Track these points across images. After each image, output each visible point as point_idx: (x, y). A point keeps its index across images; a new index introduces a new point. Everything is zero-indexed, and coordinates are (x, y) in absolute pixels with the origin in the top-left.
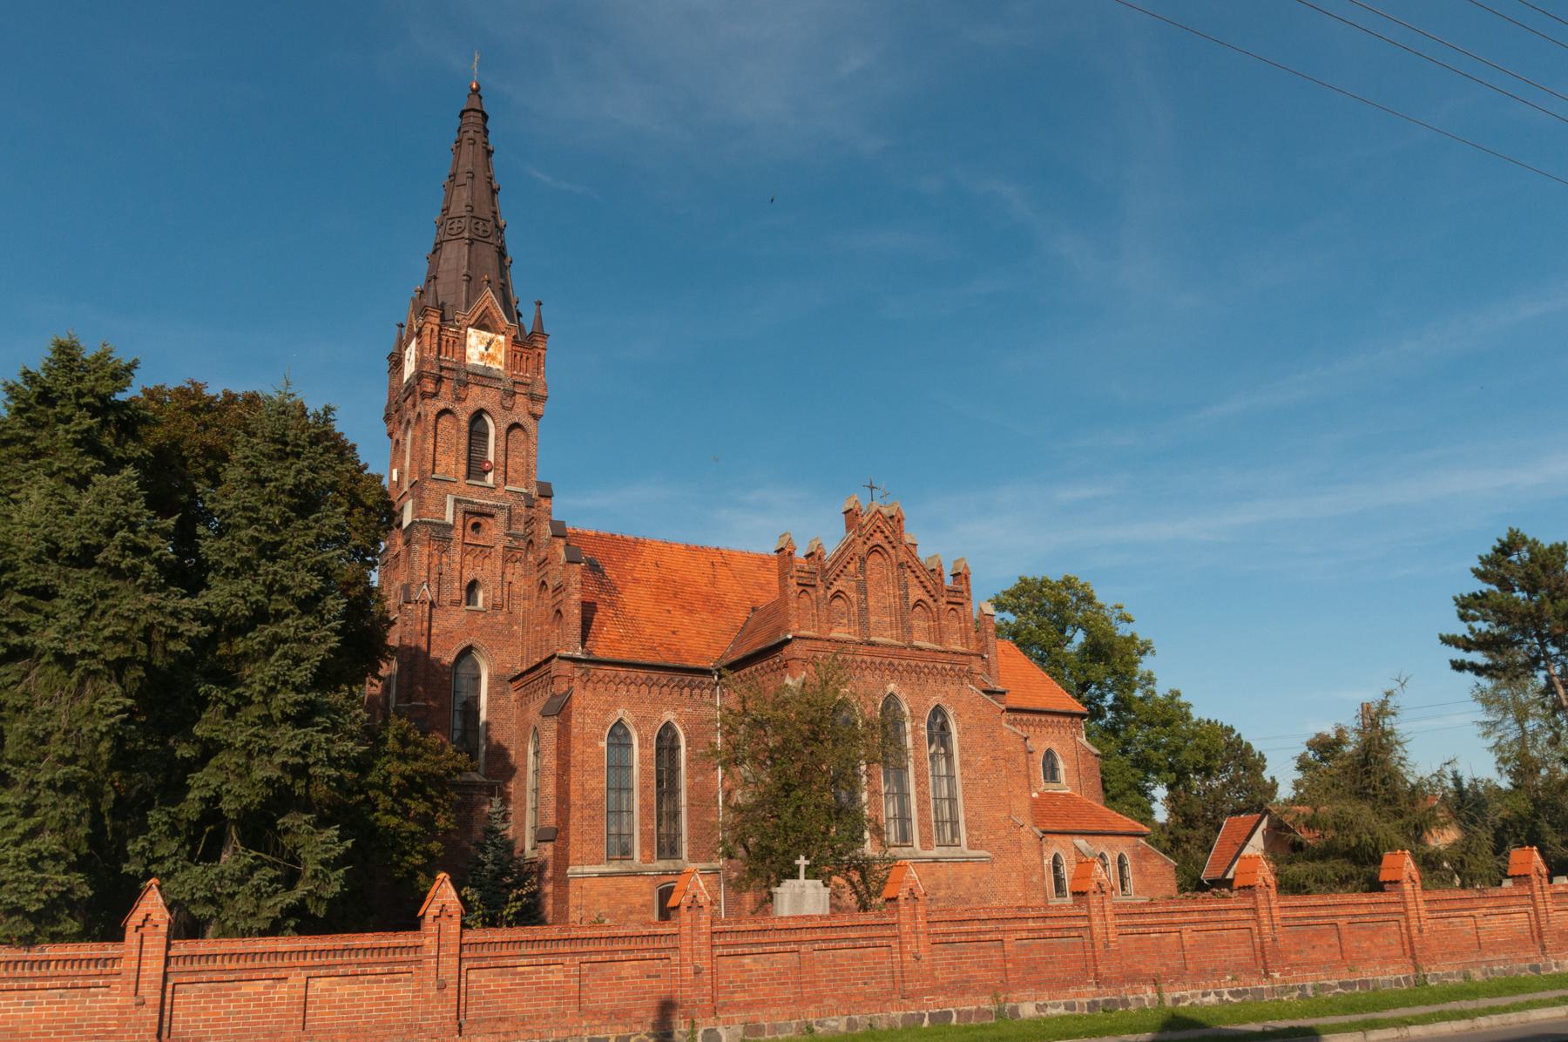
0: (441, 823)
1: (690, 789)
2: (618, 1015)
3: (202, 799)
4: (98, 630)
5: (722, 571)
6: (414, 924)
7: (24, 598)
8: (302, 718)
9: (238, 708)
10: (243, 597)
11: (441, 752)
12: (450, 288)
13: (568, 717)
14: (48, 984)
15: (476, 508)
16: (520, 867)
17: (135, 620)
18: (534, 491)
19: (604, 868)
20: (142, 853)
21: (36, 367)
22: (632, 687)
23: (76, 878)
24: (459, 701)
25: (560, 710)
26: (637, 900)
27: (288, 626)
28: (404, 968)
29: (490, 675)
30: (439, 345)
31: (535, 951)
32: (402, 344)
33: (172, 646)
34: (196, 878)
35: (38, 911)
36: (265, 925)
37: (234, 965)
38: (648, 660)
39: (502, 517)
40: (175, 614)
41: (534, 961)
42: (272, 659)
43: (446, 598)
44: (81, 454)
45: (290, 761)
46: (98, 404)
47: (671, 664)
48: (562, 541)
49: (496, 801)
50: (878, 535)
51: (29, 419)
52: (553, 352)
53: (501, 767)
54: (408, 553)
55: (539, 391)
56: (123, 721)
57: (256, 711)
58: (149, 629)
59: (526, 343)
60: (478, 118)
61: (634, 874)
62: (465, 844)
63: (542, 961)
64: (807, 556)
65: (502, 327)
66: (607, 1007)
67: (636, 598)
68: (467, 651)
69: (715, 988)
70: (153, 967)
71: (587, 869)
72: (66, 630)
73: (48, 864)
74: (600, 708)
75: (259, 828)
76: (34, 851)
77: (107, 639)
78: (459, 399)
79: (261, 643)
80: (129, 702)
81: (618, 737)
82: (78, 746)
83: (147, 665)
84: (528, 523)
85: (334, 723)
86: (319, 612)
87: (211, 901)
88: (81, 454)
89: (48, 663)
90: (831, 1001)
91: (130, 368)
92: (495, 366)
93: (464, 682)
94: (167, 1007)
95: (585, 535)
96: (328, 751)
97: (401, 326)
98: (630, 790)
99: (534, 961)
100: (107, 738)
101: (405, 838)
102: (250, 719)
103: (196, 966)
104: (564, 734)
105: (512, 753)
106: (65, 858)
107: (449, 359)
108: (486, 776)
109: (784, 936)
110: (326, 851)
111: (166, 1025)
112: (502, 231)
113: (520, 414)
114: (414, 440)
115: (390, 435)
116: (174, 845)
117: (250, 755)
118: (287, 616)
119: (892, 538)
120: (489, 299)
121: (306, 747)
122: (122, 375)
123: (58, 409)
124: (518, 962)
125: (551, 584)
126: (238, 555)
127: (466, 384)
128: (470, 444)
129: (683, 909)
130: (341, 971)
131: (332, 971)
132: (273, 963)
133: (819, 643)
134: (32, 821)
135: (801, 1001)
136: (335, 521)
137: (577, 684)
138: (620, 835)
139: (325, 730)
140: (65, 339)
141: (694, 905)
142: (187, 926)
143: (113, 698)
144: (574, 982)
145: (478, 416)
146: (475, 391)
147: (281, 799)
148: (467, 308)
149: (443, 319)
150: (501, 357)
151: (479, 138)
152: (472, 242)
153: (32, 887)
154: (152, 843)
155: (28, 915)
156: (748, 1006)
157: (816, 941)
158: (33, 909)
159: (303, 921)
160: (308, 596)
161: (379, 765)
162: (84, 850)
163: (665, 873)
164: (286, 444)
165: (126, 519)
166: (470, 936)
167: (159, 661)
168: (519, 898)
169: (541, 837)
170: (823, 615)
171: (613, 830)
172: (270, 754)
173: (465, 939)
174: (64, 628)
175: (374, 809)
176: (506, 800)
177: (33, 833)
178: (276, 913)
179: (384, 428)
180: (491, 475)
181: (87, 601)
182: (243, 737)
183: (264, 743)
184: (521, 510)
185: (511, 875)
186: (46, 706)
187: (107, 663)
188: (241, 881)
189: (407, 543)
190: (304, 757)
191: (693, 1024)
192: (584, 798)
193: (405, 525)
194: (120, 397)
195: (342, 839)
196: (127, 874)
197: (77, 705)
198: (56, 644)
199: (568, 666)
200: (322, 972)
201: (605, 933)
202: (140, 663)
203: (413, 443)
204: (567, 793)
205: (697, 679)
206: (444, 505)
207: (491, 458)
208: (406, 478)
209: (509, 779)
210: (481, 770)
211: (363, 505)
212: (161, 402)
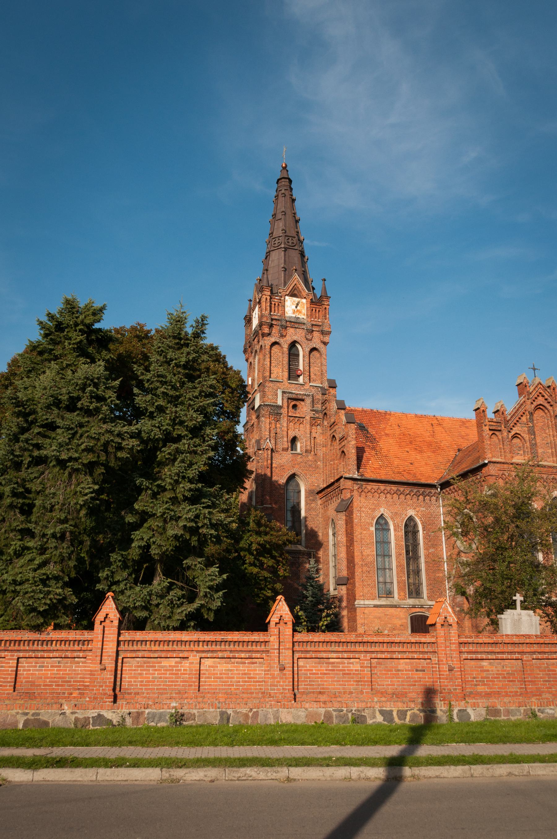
0: (281, 573)
1: (427, 556)
2: (398, 695)
3: (139, 547)
4: (79, 445)
5: (438, 429)
6: (264, 627)
7: (41, 429)
8: (194, 500)
9: (158, 493)
10: (159, 427)
11: (282, 530)
12: (275, 275)
13: (351, 513)
14: (51, 655)
15: (294, 396)
16: (328, 600)
17: (98, 440)
18: (326, 385)
19: (377, 602)
20: (107, 578)
21: (55, 311)
22: (388, 495)
23: (68, 591)
24: (290, 505)
25: (347, 508)
26: (398, 622)
27: (184, 444)
28: (258, 655)
29: (306, 490)
30: (271, 307)
31: (340, 649)
32: (251, 310)
33: (119, 454)
34: (136, 594)
35: (45, 611)
36: (177, 624)
37: (157, 648)
38: (397, 479)
39: (308, 401)
40: (119, 435)
41: (340, 655)
42: (176, 463)
43: (280, 447)
44: (78, 356)
45: (188, 525)
46: (86, 329)
47: (411, 481)
48: (343, 411)
49: (312, 561)
50: (540, 398)
51: (51, 339)
52: (332, 305)
53: (314, 543)
54: (259, 422)
55: (326, 329)
56: (92, 498)
57: (168, 495)
58: (106, 445)
59: (318, 302)
60: (285, 182)
61: (395, 606)
62: (296, 586)
63: (346, 655)
64: (495, 413)
65: (304, 294)
66: (390, 689)
67: (387, 444)
68: (292, 477)
69: (464, 681)
70: (111, 647)
71: (367, 602)
72: (60, 445)
73: (52, 583)
74: (369, 508)
75: (173, 565)
76: (44, 574)
77: (83, 450)
78: (282, 336)
79: (169, 454)
80: (96, 487)
81: (381, 525)
82: (69, 513)
83: (106, 465)
84: (323, 403)
85: (213, 503)
86: (202, 436)
87: (145, 608)
88: (78, 356)
89: (54, 466)
90: (548, 696)
91: (102, 310)
92: (301, 316)
93: (291, 494)
94: (119, 672)
95: (355, 411)
96: (210, 520)
97: (250, 301)
98: (390, 556)
99: (340, 655)
100: (84, 509)
101: (261, 580)
102: (165, 500)
103: (135, 648)
104: (349, 522)
105: (320, 534)
106: (62, 579)
107: (276, 314)
108: (306, 547)
109: (510, 648)
110: (211, 580)
111: (118, 683)
112: (302, 243)
113: (316, 343)
114: (259, 360)
115: (247, 360)
116: (125, 574)
117: (165, 521)
118: (184, 437)
119: (550, 400)
120: (297, 279)
121: (197, 516)
122: (98, 313)
123: (65, 333)
124: (330, 655)
125: (338, 436)
126: (156, 404)
127: (286, 327)
128: (289, 361)
129: (438, 626)
130: (220, 655)
131: (215, 655)
132: (179, 647)
133: (506, 466)
134: (44, 557)
135: (526, 694)
136: (210, 383)
137: (355, 493)
138: (385, 583)
139: (208, 507)
140: (69, 297)
141: (446, 624)
142: (132, 621)
143: (87, 485)
144: (367, 671)
145: (293, 345)
146: (291, 331)
147: (183, 549)
148: (285, 285)
149: (271, 291)
150: (304, 311)
151: (287, 193)
152: (286, 249)
153: (42, 596)
154: (113, 573)
155: (39, 612)
156: (488, 695)
157: (534, 653)
158: (41, 609)
159: (199, 622)
160: (195, 427)
161: (245, 538)
162: (73, 575)
163: (414, 607)
164: (180, 339)
165: (92, 380)
166: (299, 637)
167: (112, 463)
168: (328, 615)
169: (340, 582)
170: (507, 448)
171: (381, 579)
172: (177, 521)
173: (296, 639)
174: (60, 444)
175: (244, 563)
176: (317, 561)
177: (44, 564)
178: (183, 617)
179: (243, 357)
180: (301, 377)
181: (72, 429)
182: (160, 510)
183: (173, 513)
184: (319, 396)
185: (323, 604)
186: (53, 490)
187: (84, 465)
188: (162, 597)
189: (258, 417)
190: (196, 523)
191: (450, 705)
192: (363, 560)
193: (256, 407)
194: (97, 326)
195: (221, 573)
196: (99, 590)
197: (68, 489)
198: (55, 453)
199: (349, 483)
200: (209, 655)
201: (386, 639)
202: (103, 465)
203: (259, 362)
204: (353, 557)
205: (428, 491)
206: (277, 395)
207: (301, 368)
208: (256, 382)
209: (319, 549)
210: (303, 543)
211: (229, 387)
212: (123, 335)
